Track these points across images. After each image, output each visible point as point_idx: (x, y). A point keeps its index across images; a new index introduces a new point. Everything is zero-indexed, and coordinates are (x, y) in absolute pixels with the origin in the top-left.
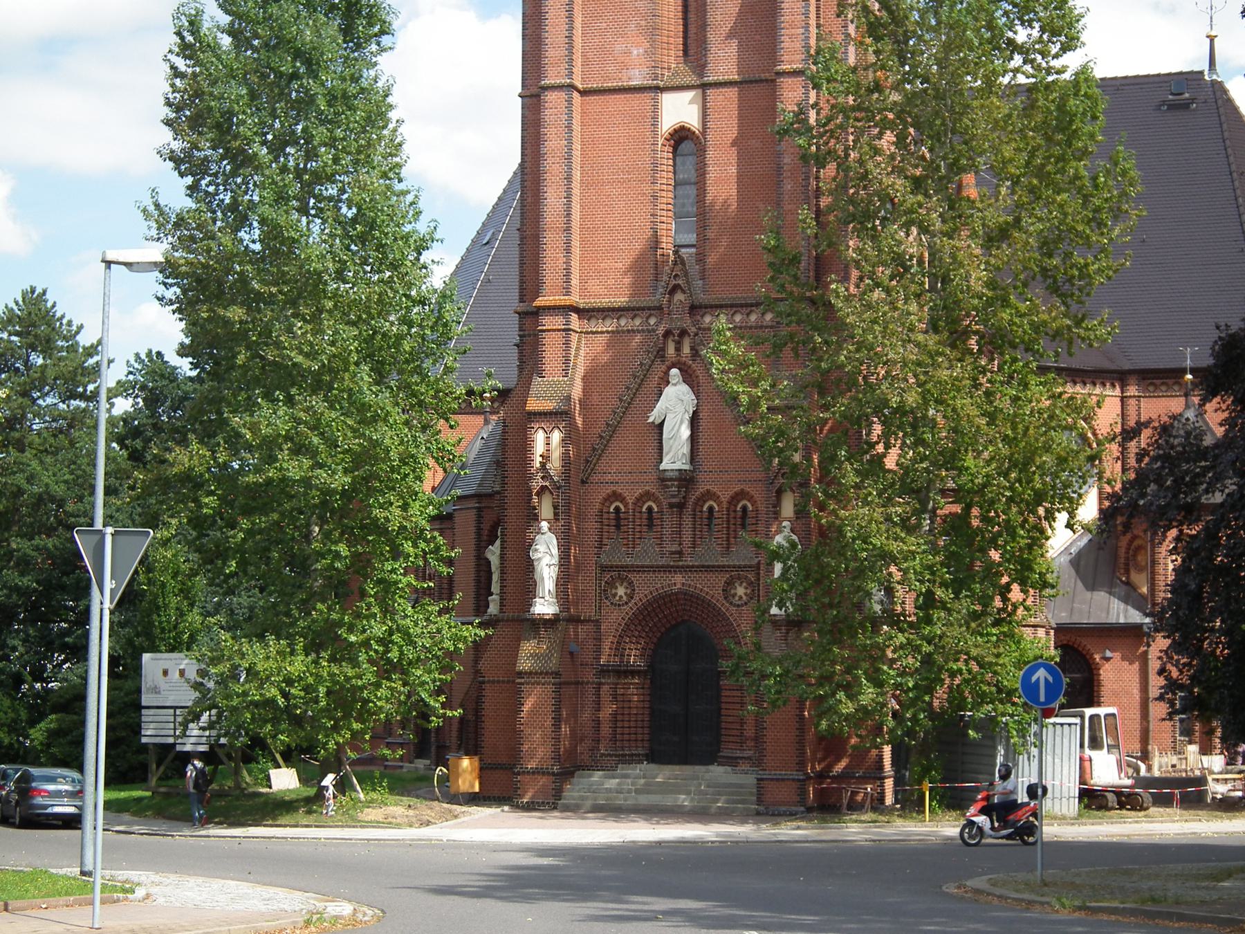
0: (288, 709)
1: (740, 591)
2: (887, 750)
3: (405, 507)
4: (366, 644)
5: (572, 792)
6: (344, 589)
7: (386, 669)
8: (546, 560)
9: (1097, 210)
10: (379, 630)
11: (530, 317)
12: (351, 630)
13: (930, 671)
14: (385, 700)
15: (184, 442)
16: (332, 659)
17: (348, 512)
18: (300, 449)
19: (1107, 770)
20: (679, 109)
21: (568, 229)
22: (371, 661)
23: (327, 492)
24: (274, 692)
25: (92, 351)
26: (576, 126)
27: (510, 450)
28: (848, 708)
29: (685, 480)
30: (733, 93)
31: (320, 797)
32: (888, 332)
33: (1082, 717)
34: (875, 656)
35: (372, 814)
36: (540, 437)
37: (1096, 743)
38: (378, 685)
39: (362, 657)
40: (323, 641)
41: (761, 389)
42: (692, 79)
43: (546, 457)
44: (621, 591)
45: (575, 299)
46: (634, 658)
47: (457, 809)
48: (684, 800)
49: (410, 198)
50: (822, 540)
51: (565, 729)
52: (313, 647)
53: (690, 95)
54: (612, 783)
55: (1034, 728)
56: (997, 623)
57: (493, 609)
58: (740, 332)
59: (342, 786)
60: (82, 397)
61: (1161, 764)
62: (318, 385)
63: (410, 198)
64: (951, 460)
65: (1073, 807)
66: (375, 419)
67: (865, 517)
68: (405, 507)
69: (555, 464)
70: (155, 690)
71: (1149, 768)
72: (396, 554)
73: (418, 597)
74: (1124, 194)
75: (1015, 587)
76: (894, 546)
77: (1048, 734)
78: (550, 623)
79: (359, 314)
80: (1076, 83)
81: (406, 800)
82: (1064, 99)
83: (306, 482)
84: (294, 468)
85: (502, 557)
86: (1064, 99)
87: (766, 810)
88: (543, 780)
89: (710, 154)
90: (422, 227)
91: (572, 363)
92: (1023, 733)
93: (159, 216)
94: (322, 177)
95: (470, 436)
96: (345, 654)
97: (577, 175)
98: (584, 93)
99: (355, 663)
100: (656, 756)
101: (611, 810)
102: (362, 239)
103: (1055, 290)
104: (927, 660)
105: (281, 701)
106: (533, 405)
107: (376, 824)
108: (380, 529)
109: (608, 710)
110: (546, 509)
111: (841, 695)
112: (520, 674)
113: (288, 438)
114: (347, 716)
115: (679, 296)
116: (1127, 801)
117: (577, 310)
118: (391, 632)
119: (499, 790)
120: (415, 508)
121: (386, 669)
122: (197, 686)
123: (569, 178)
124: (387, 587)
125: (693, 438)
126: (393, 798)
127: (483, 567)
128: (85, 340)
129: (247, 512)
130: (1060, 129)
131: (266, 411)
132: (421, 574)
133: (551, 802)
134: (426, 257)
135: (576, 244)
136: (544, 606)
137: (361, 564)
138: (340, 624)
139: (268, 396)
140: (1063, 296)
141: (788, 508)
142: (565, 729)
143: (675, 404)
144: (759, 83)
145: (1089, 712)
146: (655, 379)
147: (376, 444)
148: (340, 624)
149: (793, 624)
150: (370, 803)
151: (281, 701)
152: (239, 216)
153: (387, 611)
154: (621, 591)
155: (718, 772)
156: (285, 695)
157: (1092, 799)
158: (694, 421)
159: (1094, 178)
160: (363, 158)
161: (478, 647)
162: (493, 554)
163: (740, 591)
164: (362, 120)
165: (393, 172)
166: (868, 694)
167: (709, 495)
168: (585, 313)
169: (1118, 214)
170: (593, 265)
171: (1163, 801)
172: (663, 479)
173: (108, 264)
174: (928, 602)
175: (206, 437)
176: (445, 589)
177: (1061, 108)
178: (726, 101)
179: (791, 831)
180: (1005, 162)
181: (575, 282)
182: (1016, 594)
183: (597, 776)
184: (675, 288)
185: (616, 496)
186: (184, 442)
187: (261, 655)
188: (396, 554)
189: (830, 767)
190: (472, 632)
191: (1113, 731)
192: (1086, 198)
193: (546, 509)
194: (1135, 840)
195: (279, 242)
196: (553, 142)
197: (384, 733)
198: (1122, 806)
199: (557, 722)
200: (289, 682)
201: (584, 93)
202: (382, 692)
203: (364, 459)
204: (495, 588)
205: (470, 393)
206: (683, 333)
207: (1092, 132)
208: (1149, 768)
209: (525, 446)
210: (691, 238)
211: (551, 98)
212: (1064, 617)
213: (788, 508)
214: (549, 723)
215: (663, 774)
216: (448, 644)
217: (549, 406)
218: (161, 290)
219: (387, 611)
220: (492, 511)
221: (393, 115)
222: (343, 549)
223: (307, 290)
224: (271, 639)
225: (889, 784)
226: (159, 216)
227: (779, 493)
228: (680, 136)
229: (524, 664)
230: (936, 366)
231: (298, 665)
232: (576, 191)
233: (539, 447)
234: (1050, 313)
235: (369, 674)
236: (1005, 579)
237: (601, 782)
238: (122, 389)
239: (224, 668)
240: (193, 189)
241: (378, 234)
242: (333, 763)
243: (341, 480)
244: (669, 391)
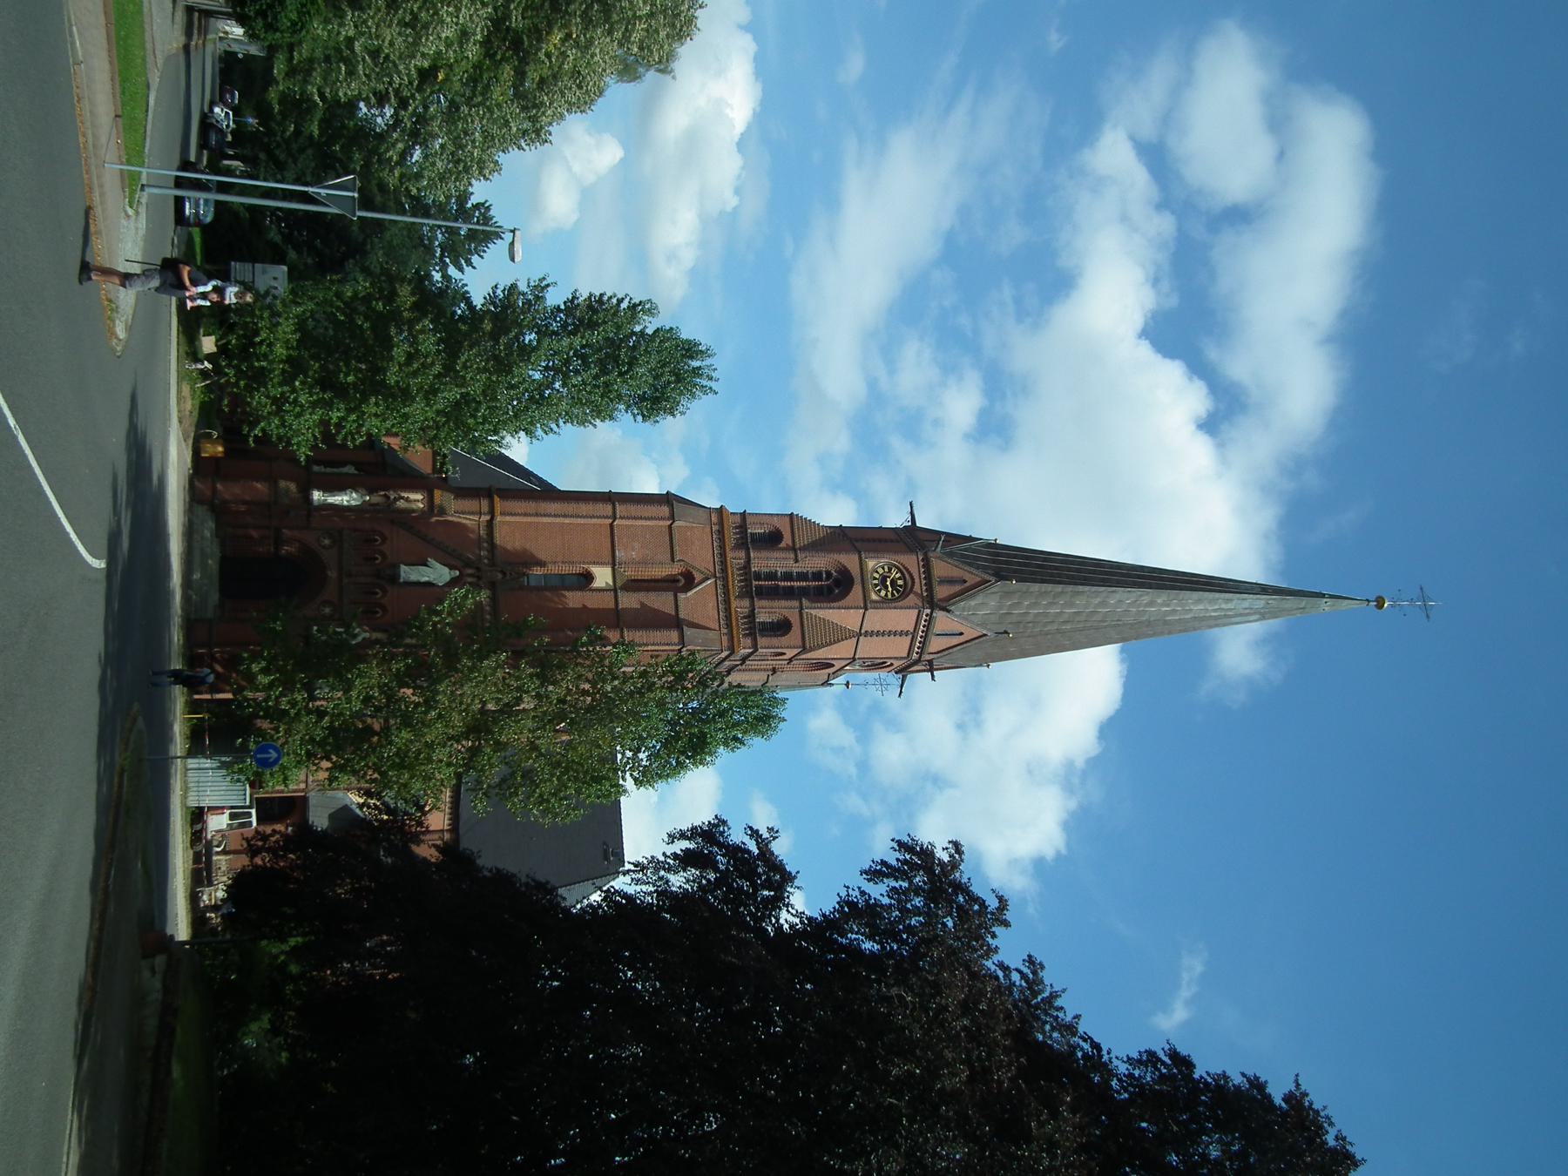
0: (253, 344)
1: (327, 610)
2: (229, 696)
3: (376, 415)
4: (294, 390)
5: (201, 510)
6: (325, 381)
7: (278, 402)
8: (346, 498)
9: (548, 801)
10: (302, 399)
11: (488, 493)
12: (302, 383)
13: (277, 715)
14: (258, 400)
15: (413, 294)
16: (284, 371)
17: (373, 385)
18: (410, 357)
19: (217, 823)
20: (603, 576)
21: (537, 515)
22: (282, 394)
23: (384, 370)
24: (264, 335)
25: (469, 263)
26: (594, 521)
27: (414, 480)
28: (255, 668)
29: (394, 578)
30: (612, 605)
31: (197, 360)
32: (482, 686)
33: (250, 807)
34: (289, 685)
35: (186, 389)
36: (419, 497)
37: (233, 817)
38: (268, 397)
39: (286, 388)
40: (295, 366)
41: (445, 616)
42: (619, 584)
43: (407, 500)
44: (327, 542)
45: (499, 518)
46: (286, 549)
47: (190, 442)
48: (196, 576)
49: (553, 426)
50: (358, 655)
51: (243, 508)
52: (288, 360)
53: (611, 582)
54: (207, 534)
55: (243, 778)
56: (308, 752)
57: (316, 468)
58: (479, 605)
59: (204, 374)
60: (442, 255)
61: (221, 861)
62: (449, 369)
63: (553, 426)
64: (407, 722)
65: (193, 802)
66: (426, 398)
67: (371, 677)
68: (376, 415)
69: (401, 504)
70: (264, 272)
71: (218, 853)
72: (349, 411)
73: (324, 423)
74: (557, 815)
75: (329, 765)
76: (354, 693)
77: (239, 786)
78: (307, 499)
79: (489, 392)
80: (618, 785)
81: (196, 413)
82: (608, 779)
83: (392, 358)
84: (399, 353)
85: (347, 474)
86: (608, 779)
87: (189, 625)
88: (209, 493)
89: (579, 594)
90: (539, 432)
91: (465, 514)
92: (240, 771)
93: (540, 288)
94: (566, 377)
95: (419, 456)
96: (287, 379)
97: (567, 521)
98: (611, 525)
99: (281, 384)
100: (224, 561)
101: (189, 532)
102: (531, 398)
103: (503, 781)
104: (285, 713)
105: (258, 339)
106: (437, 493)
107: (179, 391)
108: (364, 400)
109: (254, 534)
110: (376, 499)
111: (263, 664)
112: (276, 482)
113: (417, 350)
114: (249, 378)
115: (500, 576)
116: (197, 836)
117: (492, 518)
118: (302, 406)
119: (201, 467)
120: (375, 421)
121: (278, 402)
122: (267, 293)
123: (565, 516)
124: (329, 405)
125: (419, 584)
126: (197, 402)
127: (344, 464)
128: (475, 259)
129: (373, 328)
130: (593, 778)
131: (433, 340)
132: (339, 426)
133: (195, 497)
134: (522, 434)
135: (529, 519)
136: (317, 495)
137: (341, 391)
138: (306, 376)
139: (440, 341)
140: (499, 785)
141: (376, 635)
142: (243, 508)
143: (437, 573)
144: (617, 619)
145: (253, 811)
146: (453, 563)
147: (413, 400)
148: (306, 376)
149: (307, 638)
150: (193, 390)
151: (258, 339)
152: (543, 332)
153: (314, 405)
154: (327, 542)
155: (214, 597)
156: (262, 342)
157: (197, 816)
158: (429, 584)
159: (566, 798)
160: (576, 401)
161: (296, 461)
162: (350, 469)
163: (327, 610)
164: (594, 405)
165: (570, 418)
166: (264, 680)
167: (385, 592)
168: (490, 524)
169: (544, 813)
170: (515, 528)
171: (197, 858)
172: (396, 567)
173: (513, 231)
174: (321, 714)
175: (416, 307)
176: (328, 437)
177: (604, 778)
178: (607, 602)
179: (176, 636)
180: (575, 749)
181: (508, 518)
182: (326, 764)
183: (211, 524)
184: (504, 574)
185: (384, 539)
186: (413, 294)
187: (287, 328)
188: (349, 411)
189: (218, 662)
190: (303, 453)
191: (242, 825)
192: (555, 795)
193: (376, 499)
194: (171, 851)
195: (526, 352)
196: (584, 508)
197: (237, 401)
198: (193, 834)
199: (245, 503)
200: (270, 345)
201: (611, 525)
202: (263, 399)
203: (405, 395)
204: (329, 470)
205: (445, 456)
206: (479, 578)
207: (591, 794)
208: (218, 853)
209: (413, 488)
210: (533, 583)
211: (609, 507)
212: (312, 802)
213: (376, 635)
214: (247, 498)
215: (212, 563)
216: (295, 441)
217: (437, 501)
218: (501, 287)
219: (314, 405)
220: (378, 468)
221: (598, 422)
222: (351, 379)
223: (503, 366)
224: (297, 336)
225: (208, 697)
226: (540, 288)
227: (385, 631)
228: (589, 577)
229: (283, 484)
230: (460, 713)
231: (280, 350)
232: (558, 520)
233: (413, 496)
234: (494, 773)
235: (276, 392)
236: (334, 758)
237: (208, 528)
238: (446, 277)
239: (279, 307)
240: (558, 309)
241: (534, 411)
242: (218, 370)
243: (392, 379)
244: (446, 570)
